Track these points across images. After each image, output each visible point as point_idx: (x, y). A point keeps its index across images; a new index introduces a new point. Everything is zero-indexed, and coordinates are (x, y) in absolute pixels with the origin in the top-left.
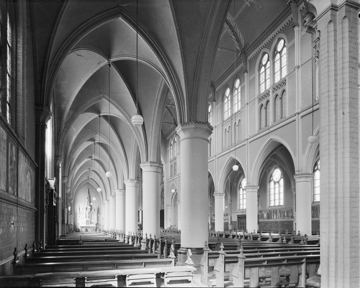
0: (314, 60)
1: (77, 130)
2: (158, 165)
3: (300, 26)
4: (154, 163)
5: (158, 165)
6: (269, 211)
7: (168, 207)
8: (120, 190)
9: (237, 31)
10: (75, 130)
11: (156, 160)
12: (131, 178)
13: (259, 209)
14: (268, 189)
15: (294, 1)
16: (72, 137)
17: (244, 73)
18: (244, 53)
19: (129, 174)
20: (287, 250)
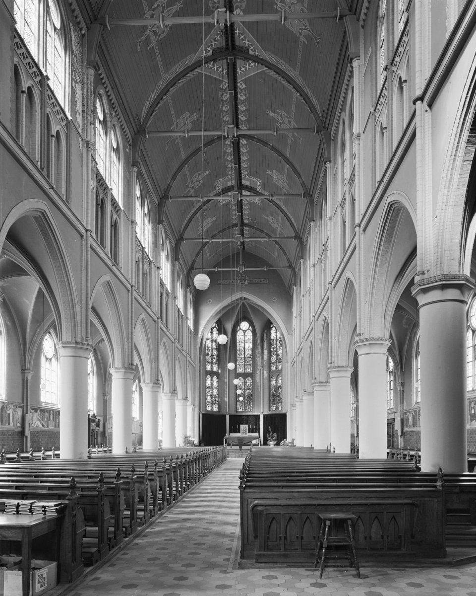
0: (373, 117)
1: (31, 302)
2: (74, 345)
3: (362, 57)
4: (67, 342)
5: (74, 345)
6: (415, 411)
7: (293, 408)
8: (155, 385)
9: (307, 92)
10: (28, 302)
11: (70, 337)
12: (117, 367)
13: (405, 408)
14: (415, 369)
15: (350, 13)
16: (28, 312)
17: (325, 164)
18: (324, 127)
19: (114, 360)
20: (37, 482)
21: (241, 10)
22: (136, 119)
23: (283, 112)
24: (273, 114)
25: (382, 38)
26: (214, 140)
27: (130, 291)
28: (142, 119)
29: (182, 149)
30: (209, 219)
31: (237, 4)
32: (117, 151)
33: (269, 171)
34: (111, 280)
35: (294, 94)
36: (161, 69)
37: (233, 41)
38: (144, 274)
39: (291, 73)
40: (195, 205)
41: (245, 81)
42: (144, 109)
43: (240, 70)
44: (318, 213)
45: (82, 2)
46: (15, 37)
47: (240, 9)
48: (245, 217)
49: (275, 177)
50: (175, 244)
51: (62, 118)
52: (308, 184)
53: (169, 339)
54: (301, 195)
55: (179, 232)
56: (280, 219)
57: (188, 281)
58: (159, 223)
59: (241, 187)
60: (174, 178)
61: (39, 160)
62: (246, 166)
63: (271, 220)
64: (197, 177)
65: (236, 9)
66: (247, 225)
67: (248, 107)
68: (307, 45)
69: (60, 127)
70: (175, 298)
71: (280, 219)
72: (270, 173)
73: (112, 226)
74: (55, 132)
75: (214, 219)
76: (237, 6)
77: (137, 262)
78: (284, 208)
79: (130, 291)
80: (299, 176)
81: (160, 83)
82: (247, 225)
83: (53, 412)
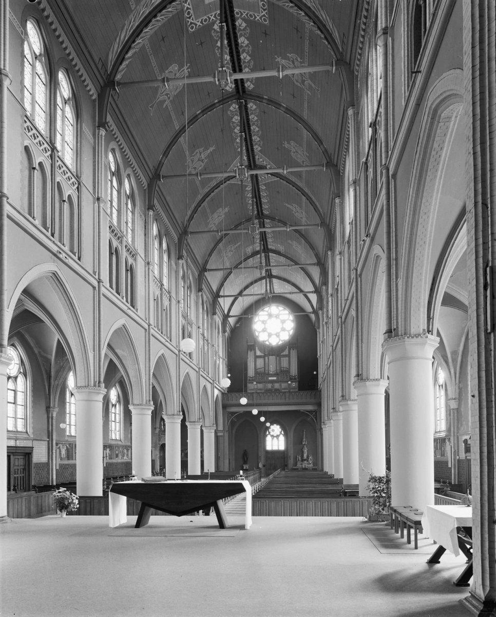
21: (245, 38)
22: (100, 66)
23: (297, 206)
24: (289, 206)
25: (369, 117)
26: (214, 104)
27: (97, 289)
28: (110, 68)
29: (174, 117)
30: (221, 209)
31: (241, 32)
32: (132, 196)
33: (286, 143)
34: (126, 324)
35: (307, 26)
36: (149, 50)
37: (254, 161)
38: (163, 310)
39: (299, 184)
40: (146, 42)
41: (265, 185)
42: (111, 53)
43: (261, 178)
44: (365, 93)
45: (55, 3)
46: (26, 122)
47: (245, 37)
48: (265, 206)
49: (293, 150)
50: (198, 275)
51: (34, 134)
52: (331, 151)
53: (173, 352)
54: (318, 225)
55: (104, 65)
56: (304, 204)
57: (199, 285)
58: (178, 259)
59: (270, 276)
60: (166, 153)
61: (50, 227)
62: (267, 207)
63: (294, 208)
64: (198, 154)
65: (243, 53)
66: (268, 217)
67: (269, 199)
68: (311, 96)
69: (72, 191)
70: (98, 199)
71: (304, 204)
72: (286, 145)
73: (127, 270)
74: (67, 198)
75: (227, 210)
76: (241, 34)
77: (155, 300)
78: (306, 190)
79: (97, 289)
80: (320, 142)
81: (130, 18)
82: (268, 217)
83: (439, 439)
